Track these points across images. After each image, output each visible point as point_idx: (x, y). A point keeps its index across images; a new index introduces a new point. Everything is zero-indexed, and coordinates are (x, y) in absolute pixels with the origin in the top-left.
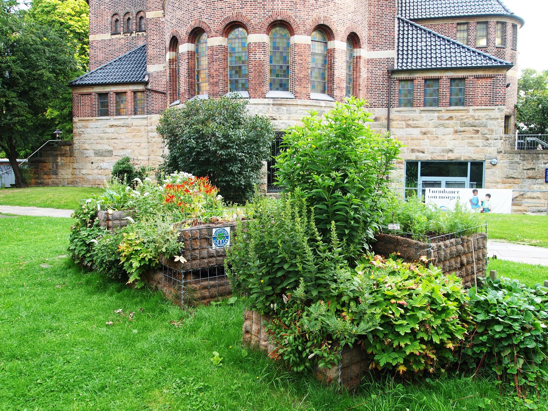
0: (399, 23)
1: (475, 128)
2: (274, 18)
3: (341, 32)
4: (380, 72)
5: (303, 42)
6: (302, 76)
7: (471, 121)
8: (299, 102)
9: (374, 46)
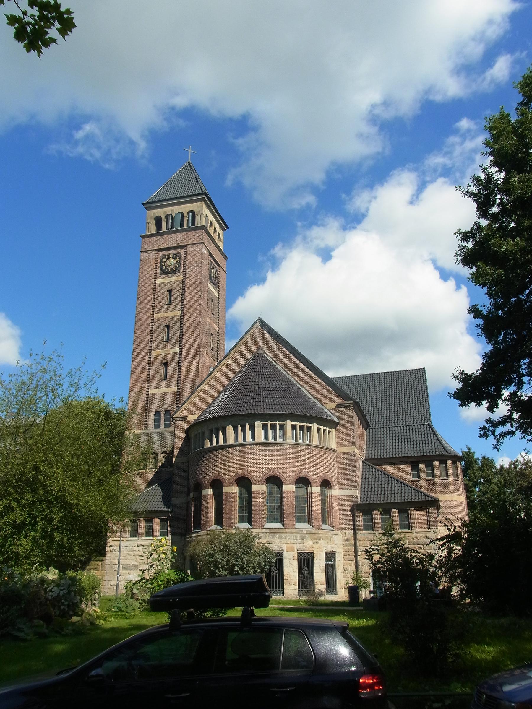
0: (363, 465)
1: (419, 546)
3: (315, 478)
5: (289, 490)
6: (289, 513)
7: (415, 540)
9: (342, 487)
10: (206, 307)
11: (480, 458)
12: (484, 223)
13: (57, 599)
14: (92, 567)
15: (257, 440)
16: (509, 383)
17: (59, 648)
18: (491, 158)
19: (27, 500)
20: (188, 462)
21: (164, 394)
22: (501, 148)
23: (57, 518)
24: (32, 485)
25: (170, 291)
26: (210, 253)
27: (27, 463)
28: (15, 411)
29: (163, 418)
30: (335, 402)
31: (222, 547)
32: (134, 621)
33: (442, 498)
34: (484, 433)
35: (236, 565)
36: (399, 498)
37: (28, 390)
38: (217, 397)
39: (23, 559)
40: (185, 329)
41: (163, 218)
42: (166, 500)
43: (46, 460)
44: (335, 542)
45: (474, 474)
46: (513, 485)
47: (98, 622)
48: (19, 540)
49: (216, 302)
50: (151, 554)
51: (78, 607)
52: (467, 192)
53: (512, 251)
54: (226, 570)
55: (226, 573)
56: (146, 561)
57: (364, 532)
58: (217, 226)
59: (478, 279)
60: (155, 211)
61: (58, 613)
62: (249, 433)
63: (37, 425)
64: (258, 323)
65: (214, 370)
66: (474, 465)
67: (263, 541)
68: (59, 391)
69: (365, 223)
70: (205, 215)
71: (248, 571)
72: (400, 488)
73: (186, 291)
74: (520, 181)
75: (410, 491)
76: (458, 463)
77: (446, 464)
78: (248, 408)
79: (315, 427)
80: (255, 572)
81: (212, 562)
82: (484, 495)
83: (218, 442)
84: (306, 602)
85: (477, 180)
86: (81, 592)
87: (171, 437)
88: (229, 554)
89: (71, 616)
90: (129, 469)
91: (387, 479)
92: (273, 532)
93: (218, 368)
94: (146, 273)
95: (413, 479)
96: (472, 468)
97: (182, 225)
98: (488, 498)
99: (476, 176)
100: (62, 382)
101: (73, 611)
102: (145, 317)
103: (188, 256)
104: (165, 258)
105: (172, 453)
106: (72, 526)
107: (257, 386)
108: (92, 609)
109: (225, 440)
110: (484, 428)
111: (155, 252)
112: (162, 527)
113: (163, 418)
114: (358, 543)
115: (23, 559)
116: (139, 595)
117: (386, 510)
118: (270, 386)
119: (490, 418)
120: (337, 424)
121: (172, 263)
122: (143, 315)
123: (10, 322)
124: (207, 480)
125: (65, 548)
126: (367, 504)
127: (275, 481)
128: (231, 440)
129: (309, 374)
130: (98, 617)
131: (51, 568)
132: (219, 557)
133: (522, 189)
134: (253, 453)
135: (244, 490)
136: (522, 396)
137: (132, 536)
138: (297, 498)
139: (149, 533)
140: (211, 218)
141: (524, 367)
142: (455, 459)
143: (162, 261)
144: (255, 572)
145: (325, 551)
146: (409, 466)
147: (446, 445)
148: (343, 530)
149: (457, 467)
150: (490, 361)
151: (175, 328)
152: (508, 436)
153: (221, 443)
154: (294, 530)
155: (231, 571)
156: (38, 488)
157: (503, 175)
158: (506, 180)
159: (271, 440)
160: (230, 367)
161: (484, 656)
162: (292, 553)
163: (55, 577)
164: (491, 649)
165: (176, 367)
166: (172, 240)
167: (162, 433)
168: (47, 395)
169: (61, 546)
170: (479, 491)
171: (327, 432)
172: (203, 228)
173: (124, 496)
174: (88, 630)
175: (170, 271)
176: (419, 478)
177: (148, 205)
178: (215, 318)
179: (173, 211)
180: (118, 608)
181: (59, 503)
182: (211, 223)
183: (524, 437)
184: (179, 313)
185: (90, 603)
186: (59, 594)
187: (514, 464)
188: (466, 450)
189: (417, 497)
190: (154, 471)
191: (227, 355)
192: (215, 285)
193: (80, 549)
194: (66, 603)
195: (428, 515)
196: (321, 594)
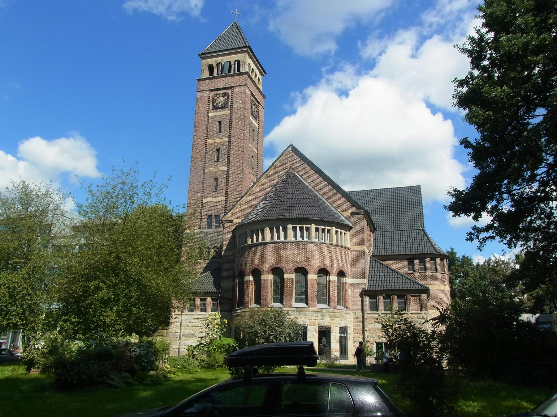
2: (298, 266)
3: (333, 270)
4: (358, 291)
8: (311, 309)
10: (248, 135)
11: (461, 257)
12: (476, 73)
13: (139, 357)
14: (159, 334)
15: (289, 239)
16: (492, 198)
17: (145, 394)
18: (484, 21)
19: (112, 282)
20: (234, 255)
21: (215, 202)
22: (492, 14)
23: (134, 296)
24: (115, 270)
25: (220, 123)
26: (251, 93)
27: (111, 253)
28: (101, 213)
29: (214, 220)
30: (349, 210)
31: (260, 321)
32: (197, 376)
33: (432, 287)
34: (471, 237)
35: (271, 335)
36: (398, 286)
37: (111, 197)
38: (257, 205)
39: (108, 326)
40: (232, 152)
41: (215, 65)
42: (217, 283)
43: (126, 252)
44: (348, 320)
45: (456, 269)
46: (486, 279)
47: (169, 375)
48: (106, 312)
49: (256, 131)
50: (208, 325)
51: (154, 363)
52: (463, 49)
53: (500, 97)
54: (263, 338)
55: (263, 341)
56: (203, 330)
57: (370, 312)
58: (258, 72)
59: (470, 118)
60: (209, 60)
61: (139, 368)
62: (282, 234)
63: (118, 224)
64: (290, 148)
65: (254, 184)
66: (456, 262)
67: (292, 317)
68: (135, 199)
69: (374, 72)
70: (248, 64)
71: (280, 340)
72: (399, 279)
73: (233, 122)
74: (508, 40)
75: (407, 281)
76: (445, 260)
77: (435, 260)
78: (284, 214)
79: (333, 229)
80: (286, 341)
81: (253, 332)
82: (463, 285)
83: (257, 240)
84: (325, 365)
85: (472, 39)
86: (156, 353)
87: (220, 236)
88: (266, 327)
89: (149, 370)
90: (190, 259)
91: (389, 271)
92: (299, 310)
93: (258, 183)
94: (201, 108)
95: (409, 272)
96: (454, 265)
97: (230, 71)
98: (467, 288)
99: (471, 36)
100: (137, 192)
101: (150, 367)
102: (200, 142)
103: (235, 95)
104: (216, 96)
105: (221, 248)
106: (146, 302)
107: (288, 197)
108: (164, 366)
109: (263, 238)
110: (471, 234)
111: (208, 92)
112: (213, 304)
113: (214, 220)
114: (365, 320)
115: (108, 326)
116: (198, 356)
117: (388, 295)
118: (300, 197)
119: (475, 226)
120: (351, 228)
121: (222, 100)
122: (199, 141)
123: (89, 145)
124: (248, 269)
125: (141, 319)
126: (373, 290)
127: (302, 271)
128: (268, 238)
129: (329, 188)
130: (169, 372)
131: (134, 334)
132: (258, 328)
133: (509, 47)
134: (285, 249)
135: (277, 277)
136: (502, 209)
137: (189, 311)
138: (318, 284)
139: (203, 309)
140: (253, 66)
141: (504, 186)
142: (443, 257)
143: (213, 99)
144: (286, 341)
145: (340, 326)
146: (406, 262)
147: (436, 246)
148: (353, 310)
149: (444, 263)
150: (479, 182)
151: (223, 151)
152: (490, 240)
153: (260, 240)
154: (316, 310)
155: (267, 340)
156: (119, 273)
157: (492, 34)
158: (496, 39)
159: (299, 239)
160: (268, 182)
161: (470, 409)
162: (314, 327)
163: (137, 341)
164: (476, 404)
165: (224, 181)
166: (222, 83)
167: (213, 232)
168: (126, 202)
169: (138, 318)
170: (459, 282)
171: (343, 234)
172: (247, 73)
173: (186, 280)
174: (163, 381)
175: (220, 106)
176: (414, 271)
177: (203, 56)
178: (255, 144)
179: (222, 60)
180: (182, 365)
181: (136, 284)
182: (253, 70)
183: (502, 241)
184: (227, 139)
185: (161, 361)
186: (140, 353)
187: (488, 262)
188: (450, 250)
189: (412, 286)
190: (207, 261)
191: (265, 173)
192: (256, 118)
193: (152, 320)
194: (146, 361)
195: (421, 301)
196: (337, 359)
